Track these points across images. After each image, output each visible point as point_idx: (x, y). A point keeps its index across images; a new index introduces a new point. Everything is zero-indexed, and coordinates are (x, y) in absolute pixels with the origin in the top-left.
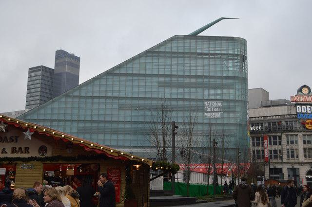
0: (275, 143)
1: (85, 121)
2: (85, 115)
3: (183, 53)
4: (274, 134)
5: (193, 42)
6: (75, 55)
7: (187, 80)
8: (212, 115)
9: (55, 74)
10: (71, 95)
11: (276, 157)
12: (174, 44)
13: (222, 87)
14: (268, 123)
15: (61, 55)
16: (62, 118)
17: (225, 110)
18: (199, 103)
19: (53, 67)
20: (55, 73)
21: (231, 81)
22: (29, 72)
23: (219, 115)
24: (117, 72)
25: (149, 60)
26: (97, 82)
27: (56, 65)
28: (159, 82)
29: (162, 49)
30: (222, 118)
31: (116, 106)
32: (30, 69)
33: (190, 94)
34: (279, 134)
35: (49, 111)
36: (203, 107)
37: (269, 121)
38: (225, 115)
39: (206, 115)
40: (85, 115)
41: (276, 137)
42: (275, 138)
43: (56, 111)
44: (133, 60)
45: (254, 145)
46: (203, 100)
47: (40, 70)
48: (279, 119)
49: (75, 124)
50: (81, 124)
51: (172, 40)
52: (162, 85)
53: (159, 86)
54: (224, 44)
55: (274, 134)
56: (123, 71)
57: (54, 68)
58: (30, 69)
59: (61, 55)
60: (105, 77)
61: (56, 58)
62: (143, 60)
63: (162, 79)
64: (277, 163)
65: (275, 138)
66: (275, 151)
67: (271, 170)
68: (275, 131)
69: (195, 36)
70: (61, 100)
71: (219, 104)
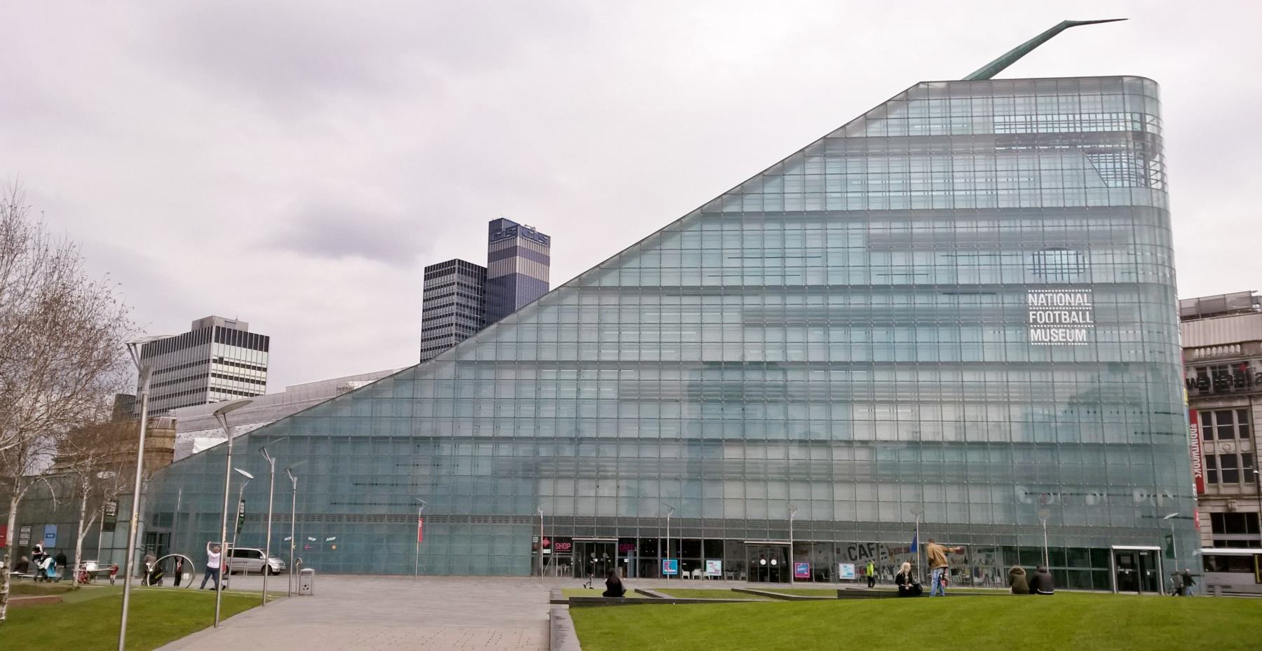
0: (1226, 434)
1: (639, 365)
2: (516, 420)
3: (948, 139)
4: (1221, 404)
5: (978, 104)
6: (538, 230)
7: (962, 227)
8: (1058, 335)
9: (493, 281)
10: (596, 284)
11: (1231, 477)
12: (915, 109)
13: (1082, 244)
14: (1198, 369)
15: (501, 232)
16: (570, 356)
17: (1098, 320)
18: (1009, 300)
19: (484, 263)
20: (490, 276)
21: (1116, 225)
22: (427, 278)
23: (1080, 335)
24: (732, 208)
25: (834, 167)
26: (671, 244)
27: (492, 257)
28: (744, 312)
29: (875, 130)
30: (1094, 344)
31: (733, 317)
32: (427, 269)
33: (805, 345)
34: (1239, 403)
35: (529, 336)
36: (1025, 310)
37: (1201, 364)
38: (1103, 335)
39: (1036, 335)
40: (516, 420)
41: (1230, 413)
42: (1224, 416)
43: (549, 336)
44: (779, 171)
45: (1208, 435)
46: (1019, 289)
47: (452, 271)
48: (1236, 356)
49: (609, 374)
50: (629, 375)
51: (907, 97)
52: (754, 321)
53: (745, 325)
54: (1089, 102)
55: (1221, 404)
56: (751, 206)
57: (485, 266)
58: (427, 269)
59: (501, 232)
60: (697, 227)
61: (490, 240)
62: (813, 168)
63: (877, 228)
64: (1239, 497)
65: (1224, 416)
66: (1229, 459)
67: (1216, 518)
68: (1221, 390)
69: (984, 79)
70: (565, 302)
71: (1081, 299)
